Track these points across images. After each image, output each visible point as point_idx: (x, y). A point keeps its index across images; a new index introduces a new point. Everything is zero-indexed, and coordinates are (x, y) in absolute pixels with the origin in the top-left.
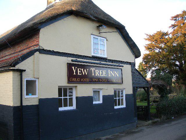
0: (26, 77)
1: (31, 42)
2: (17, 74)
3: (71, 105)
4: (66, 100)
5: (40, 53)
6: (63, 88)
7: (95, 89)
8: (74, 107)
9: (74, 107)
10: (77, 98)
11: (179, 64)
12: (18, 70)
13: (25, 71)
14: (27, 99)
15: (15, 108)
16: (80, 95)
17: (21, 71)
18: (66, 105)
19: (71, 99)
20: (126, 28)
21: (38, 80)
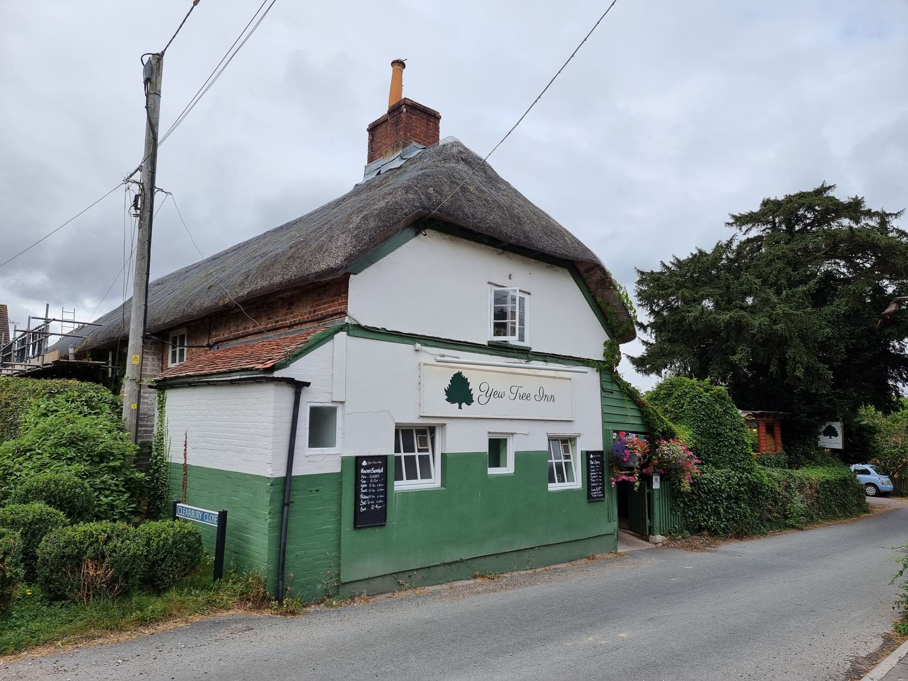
0: (309, 400)
1: (324, 303)
2: (287, 394)
3: (426, 474)
4: (410, 461)
5: (348, 334)
6: (428, 456)
7: (197, 101)
8: (434, 482)
9: (434, 482)
10: (444, 456)
11: (654, 342)
12: (290, 382)
13: (308, 384)
14: (311, 459)
15: (275, 482)
16: (449, 450)
17: (298, 386)
18: (412, 476)
19: (425, 461)
20: (403, 91)
21: (343, 407)
